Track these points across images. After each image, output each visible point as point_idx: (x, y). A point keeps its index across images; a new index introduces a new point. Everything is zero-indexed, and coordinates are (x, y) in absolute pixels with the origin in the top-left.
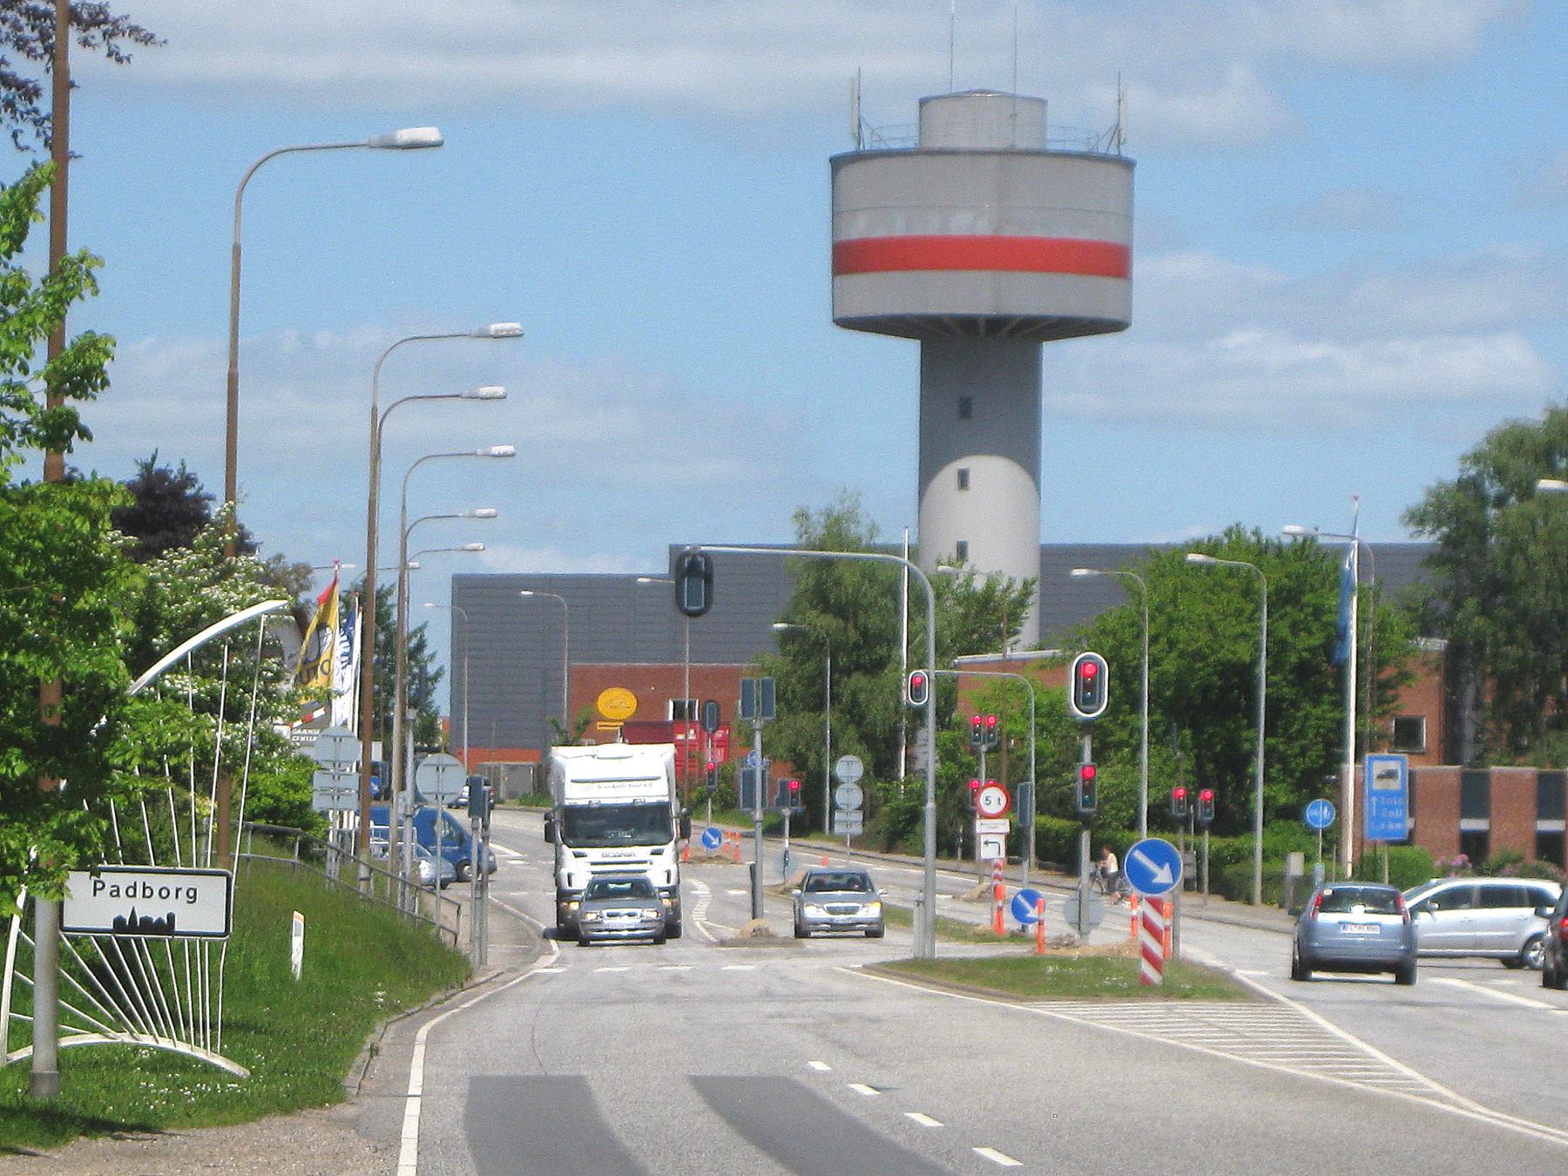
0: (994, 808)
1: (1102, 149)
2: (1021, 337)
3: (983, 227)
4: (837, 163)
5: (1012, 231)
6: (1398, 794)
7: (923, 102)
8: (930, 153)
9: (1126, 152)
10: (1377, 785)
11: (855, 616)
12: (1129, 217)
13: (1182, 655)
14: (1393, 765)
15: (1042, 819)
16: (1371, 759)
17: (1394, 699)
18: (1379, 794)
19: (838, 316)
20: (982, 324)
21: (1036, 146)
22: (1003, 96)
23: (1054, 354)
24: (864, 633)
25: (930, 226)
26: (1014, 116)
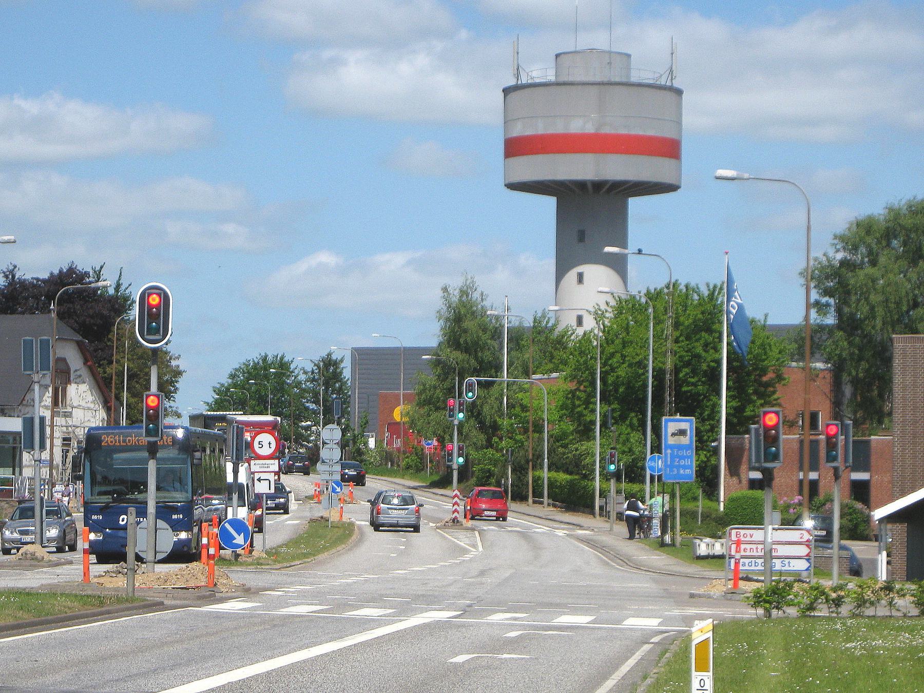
0: (266, 451)
1: (662, 82)
2: (617, 193)
3: (590, 129)
4: (507, 91)
5: (607, 130)
6: (687, 447)
7: (557, 56)
8: (564, 84)
9: (676, 84)
10: (671, 441)
11: (476, 351)
12: (679, 123)
13: (630, 365)
14: (684, 426)
15: (554, 474)
16: (667, 421)
17: (774, 392)
18: (672, 447)
19: (507, 182)
20: (590, 186)
21: (624, 80)
22: (603, 52)
23: (635, 204)
24: (481, 362)
25: (558, 128)
26: (610, 63)
